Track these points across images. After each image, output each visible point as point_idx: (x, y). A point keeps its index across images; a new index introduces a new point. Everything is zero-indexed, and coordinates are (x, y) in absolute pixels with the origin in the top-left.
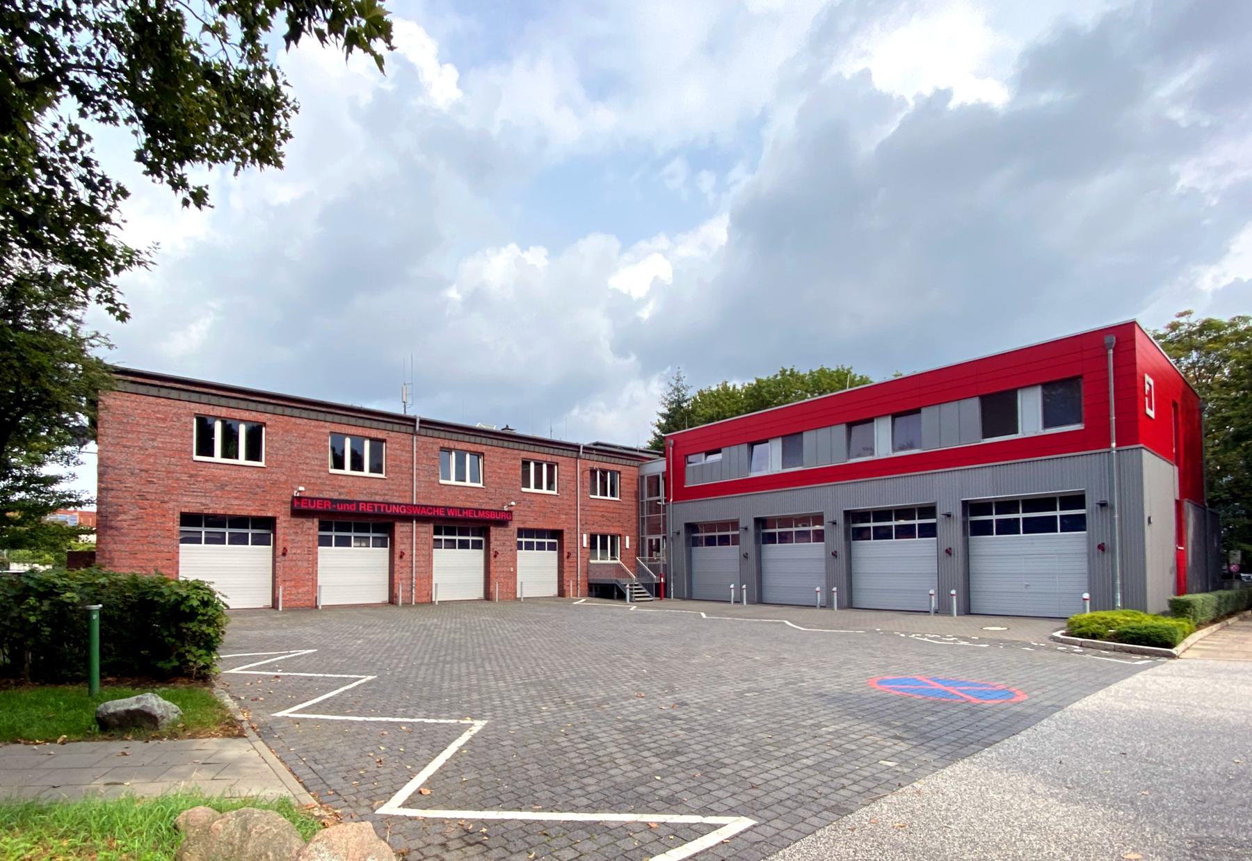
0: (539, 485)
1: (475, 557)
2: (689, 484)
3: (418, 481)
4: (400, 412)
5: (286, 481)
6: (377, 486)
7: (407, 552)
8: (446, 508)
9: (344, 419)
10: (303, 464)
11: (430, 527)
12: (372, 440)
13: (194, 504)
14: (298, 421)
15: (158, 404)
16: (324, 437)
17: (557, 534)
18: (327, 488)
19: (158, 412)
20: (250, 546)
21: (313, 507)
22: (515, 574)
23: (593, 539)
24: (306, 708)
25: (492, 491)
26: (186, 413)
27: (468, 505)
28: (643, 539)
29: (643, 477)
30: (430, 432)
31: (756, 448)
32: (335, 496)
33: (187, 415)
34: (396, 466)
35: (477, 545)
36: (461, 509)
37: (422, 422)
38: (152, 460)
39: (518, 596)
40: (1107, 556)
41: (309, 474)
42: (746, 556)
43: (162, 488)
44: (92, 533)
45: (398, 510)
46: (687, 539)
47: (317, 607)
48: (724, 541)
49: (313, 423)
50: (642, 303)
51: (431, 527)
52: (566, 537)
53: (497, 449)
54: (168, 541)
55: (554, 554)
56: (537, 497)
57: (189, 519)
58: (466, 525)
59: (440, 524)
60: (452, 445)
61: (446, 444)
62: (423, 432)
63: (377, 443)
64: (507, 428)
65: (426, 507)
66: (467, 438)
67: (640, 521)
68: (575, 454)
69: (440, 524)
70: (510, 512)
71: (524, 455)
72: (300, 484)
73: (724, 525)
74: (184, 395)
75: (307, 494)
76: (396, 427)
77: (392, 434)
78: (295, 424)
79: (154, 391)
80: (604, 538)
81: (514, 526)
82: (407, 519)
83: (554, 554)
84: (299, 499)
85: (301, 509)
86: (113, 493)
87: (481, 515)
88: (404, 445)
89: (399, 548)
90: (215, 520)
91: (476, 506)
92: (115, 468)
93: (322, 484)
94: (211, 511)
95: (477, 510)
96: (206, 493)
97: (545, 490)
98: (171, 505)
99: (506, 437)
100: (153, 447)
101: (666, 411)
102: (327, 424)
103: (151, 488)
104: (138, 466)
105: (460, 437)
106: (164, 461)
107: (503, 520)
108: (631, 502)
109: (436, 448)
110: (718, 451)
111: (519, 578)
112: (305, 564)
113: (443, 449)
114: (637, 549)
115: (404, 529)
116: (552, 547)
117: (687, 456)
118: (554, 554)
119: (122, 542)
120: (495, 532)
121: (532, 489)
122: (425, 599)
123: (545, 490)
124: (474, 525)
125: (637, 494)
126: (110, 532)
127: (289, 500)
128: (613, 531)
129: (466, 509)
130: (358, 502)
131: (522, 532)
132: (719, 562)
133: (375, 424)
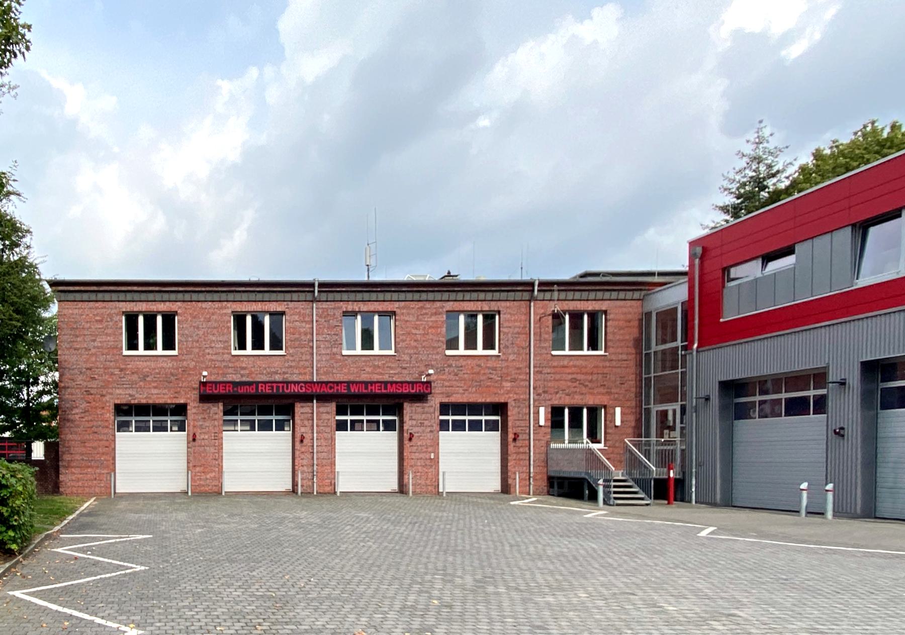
0: (471, 343)
1: (385, 442)
2: (729, 315)
3: (318, 354)
4: (364, 278)
5: (195, 367)
6: (277, 363)
7: (308, 436)
8: (349, 383)
9: (245, 296)
10: (212, 348)
12: (272, 314)
13: (123, 396)
14: (204, 305)
15: (97, 308)
17: (500, 408)
18: (230, 371)
19: (97, 315)
20: (274, 432)
21: (216, 392)
22: (436, 461)
23: (556, 413)
24: (34, 592)
25: (407, 358)
26: (115, 312)
27: (376, 378)
28: (648, 411)
29: (648, 314)
30: (331, 296)
31: (872, 231)
32: (237, 378)
33: (117, 314)
34: (296, 340)
35: (389, 426)
36: (366, 383)
37: (321, 285)
38: (93, 359)
39: (441, 490)
40: (702, 394)
41: (214, 357)
42: (839, 433)
43: (101, 384)
45: (295, 389)
46: (723, 408)
47: (335, 493)
48: (797, 407)
49: (217, 305)
50: (787, 39)
51: (333, 406)
52: (512, 412)
53: (412, 305)
54: (106, 431)
55: (495, 437)
56: (463, 361)
57: (121, 410)
58: (375, 402)
59: (345, 402)
60: (356, 307)
61: (350, 307)
62: (324, 296)
63: (277, 316)
64: (449, 275)
65: (327, 383)
66: (374, 296)
67: (642, 385)
68: (526, 295)
69: (345, 402)
70: (428, 383)
71: (557, 307)
73: (797, 380)
74: (114, 296)
75: (213, 378)
76: (295, 296)
77: (291, 305)
78: (201, 308)
79: (93, 296)
80: (576, 413)
81: (435, 401)
82: (307, 398)
83: (496, 435)
84: (203, 384)
85: (209, 394)
86: (69, 390)
87: (391, 390)
88: (304, 315)
89: (300, 430)
90: (142, 410)
91: (386, 378)
92: (70, 369)
93: (227, 367)
94: (136, 402)
95: (386, 383)
96: (132, 384)
97: (480, 351)
98: (107, 398)
99: (449, 287)
100: (94, 347)
101: (730, 200)
102: (229, 305)
103: (94, 384)
104: (84, 366)
105: (366, 296)
106: (102, 358)
107: (419, 394)
108: (626, 355)
109: (339, 313)
110: (789, 251)
111: (442, 468)
112: (212, 450)
113: (346, 314)
114: (638, 426)
116: (492, 426)
117: (726, 270)
118: (496, 435)
119: (76, 433)
120: (409, 409)
121: (462, 351)
122: (328, 489)
123: (480, 351)
124: (385, 402)
125: (638, 343)
126: (68, 424)
127: (197, 386)
128: (591, 401)
129: (372, 383)
130: (257, 383)
131: (445, 408)
132: (784, 443)
133: (274, 296)
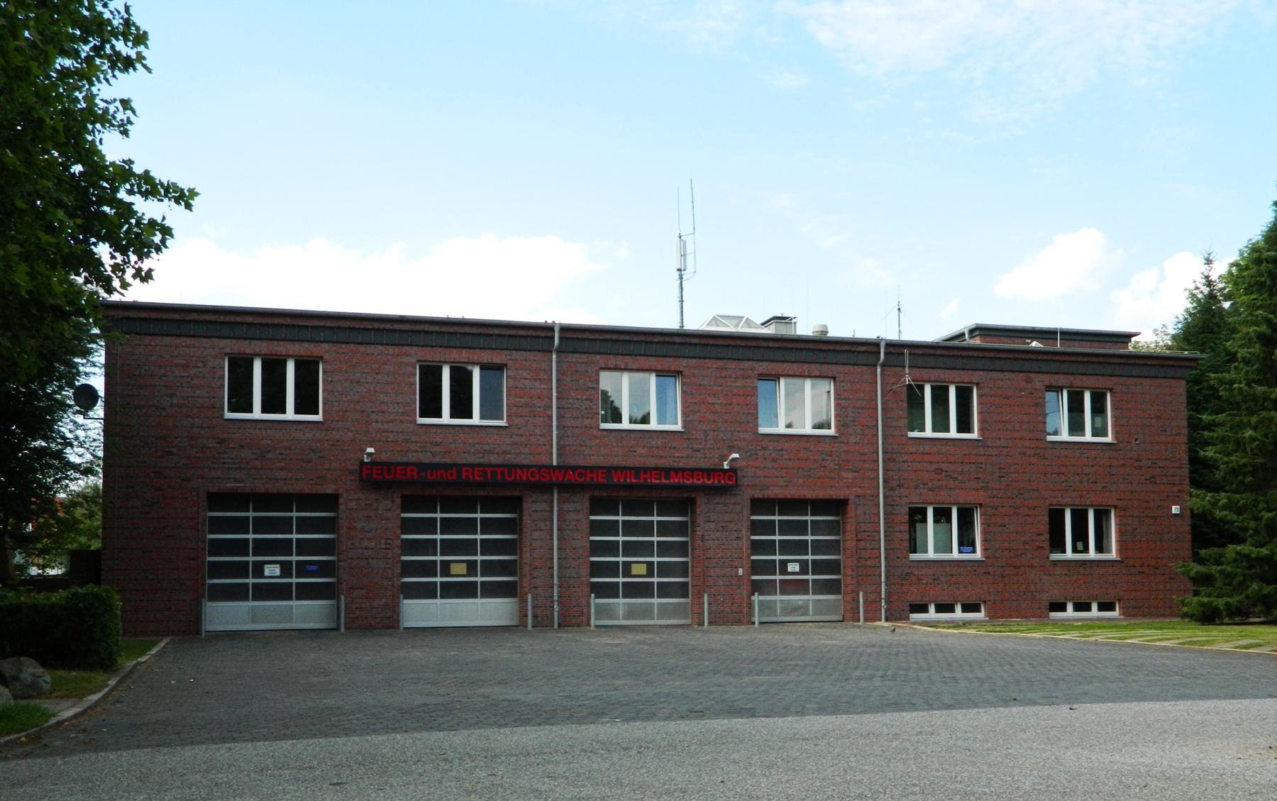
11: (581, 502)
14: (370, 349)
16: (409, 369)
32: (426, 458)
34: (526, 405)
44: (97, 536)
70: (733, 470)
72: (732, 449)
77: (515, 355)
107: (722, 483)
115: (538, 506)
120: (704, 507)
